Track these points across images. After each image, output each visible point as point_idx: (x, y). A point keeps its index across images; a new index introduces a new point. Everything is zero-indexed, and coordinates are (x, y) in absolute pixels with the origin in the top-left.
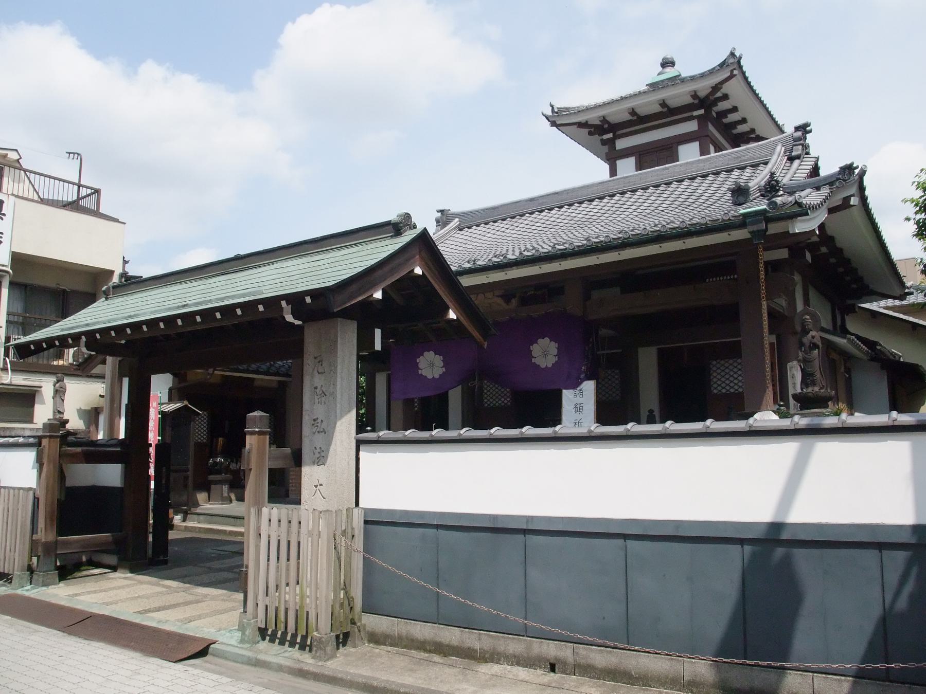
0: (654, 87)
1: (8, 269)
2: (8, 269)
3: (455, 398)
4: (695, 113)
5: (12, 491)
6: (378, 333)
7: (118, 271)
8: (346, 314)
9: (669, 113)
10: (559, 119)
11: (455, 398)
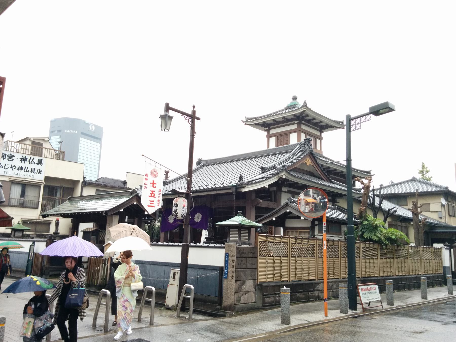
0: (288, 108)
1: (43, 182)
2: (43, 182)
3: (162, 235)
4: (296, 122)
5: (50, 157)
6: (127, 217)
7: (82, 180)
8: (116, 214)
9: (286, 121)
10: (249, 122)
11: (162, 235)
